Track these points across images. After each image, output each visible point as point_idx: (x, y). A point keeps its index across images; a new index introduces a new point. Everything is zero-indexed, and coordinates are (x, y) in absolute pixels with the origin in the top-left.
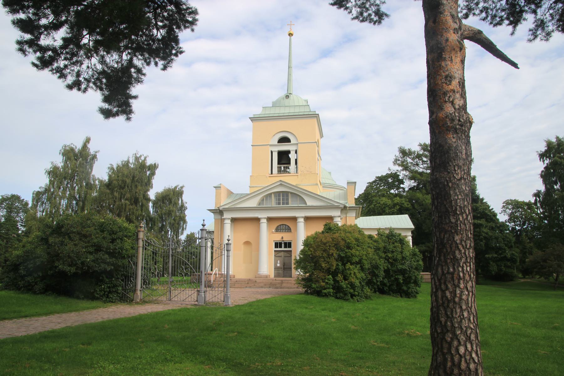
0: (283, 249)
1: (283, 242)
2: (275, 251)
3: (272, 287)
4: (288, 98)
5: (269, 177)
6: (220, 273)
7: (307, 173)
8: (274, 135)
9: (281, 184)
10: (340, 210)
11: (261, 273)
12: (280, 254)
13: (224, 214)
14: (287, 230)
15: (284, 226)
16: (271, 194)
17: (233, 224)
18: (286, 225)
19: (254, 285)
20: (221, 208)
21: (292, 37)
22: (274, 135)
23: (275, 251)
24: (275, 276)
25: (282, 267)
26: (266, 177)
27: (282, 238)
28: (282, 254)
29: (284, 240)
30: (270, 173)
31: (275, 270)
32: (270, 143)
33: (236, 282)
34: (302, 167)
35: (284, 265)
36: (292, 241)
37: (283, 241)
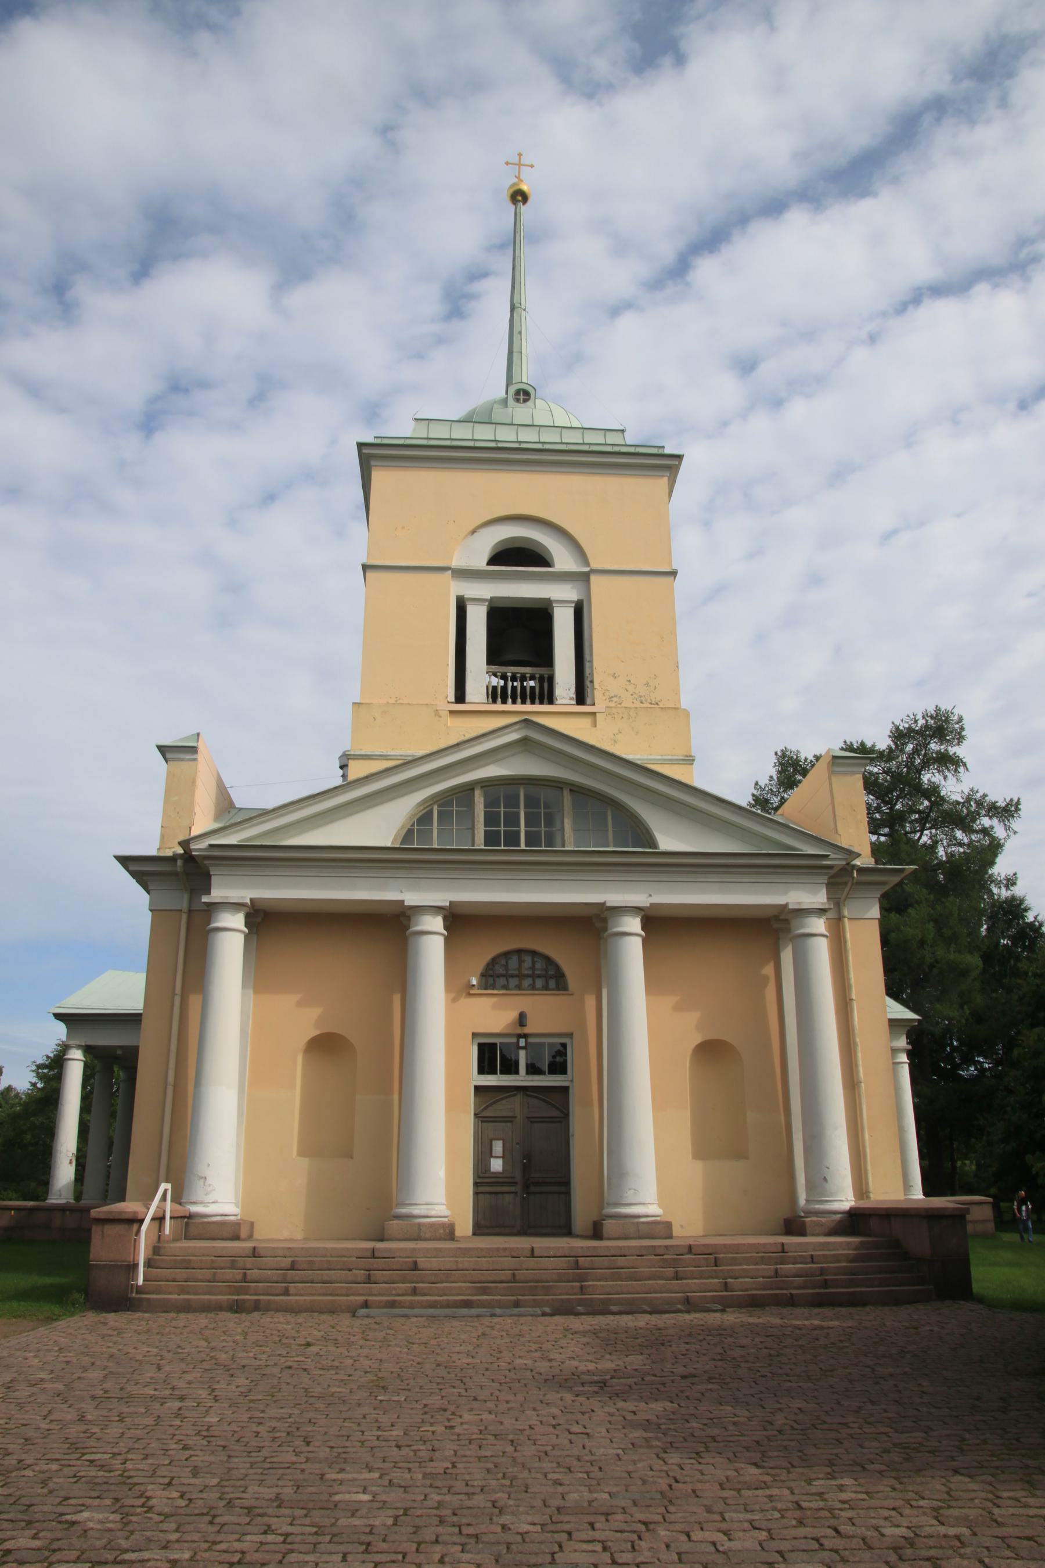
0: (522, 1079)
1: (522, 1043)
2: (478, 1089)
3: (536, 1304)
4: (525, 401)
5: (451, 712)
6: (180, 1210)
7: (638, 704)
8: (474, 532)
9: (525, 741)
10: (824, 880)
11: (416, 1211)
12: (503, 1108)
13: (214, 880)
14: (527, 982)
15: (528, 961)
16: (468, 789)
17: (255, 937)
18: (534, 953)
19: (414, 1292)
20: (198, 847)
21: (523, 208)
22: (474, 532)
23: (478, 1089)
24: (479, 1229)
25: (518, 1175)
26: (437, 713)
27: (522, 1020)
28: (515, 1106)
29: (527, 1030)
30: (452, 698)
31: (476, 1194)
32: (455, 563)
33: (292, 1268)
34: (614, 676)
35: (526, 1168)
36: (570, 1035)
37: (525, 1036)
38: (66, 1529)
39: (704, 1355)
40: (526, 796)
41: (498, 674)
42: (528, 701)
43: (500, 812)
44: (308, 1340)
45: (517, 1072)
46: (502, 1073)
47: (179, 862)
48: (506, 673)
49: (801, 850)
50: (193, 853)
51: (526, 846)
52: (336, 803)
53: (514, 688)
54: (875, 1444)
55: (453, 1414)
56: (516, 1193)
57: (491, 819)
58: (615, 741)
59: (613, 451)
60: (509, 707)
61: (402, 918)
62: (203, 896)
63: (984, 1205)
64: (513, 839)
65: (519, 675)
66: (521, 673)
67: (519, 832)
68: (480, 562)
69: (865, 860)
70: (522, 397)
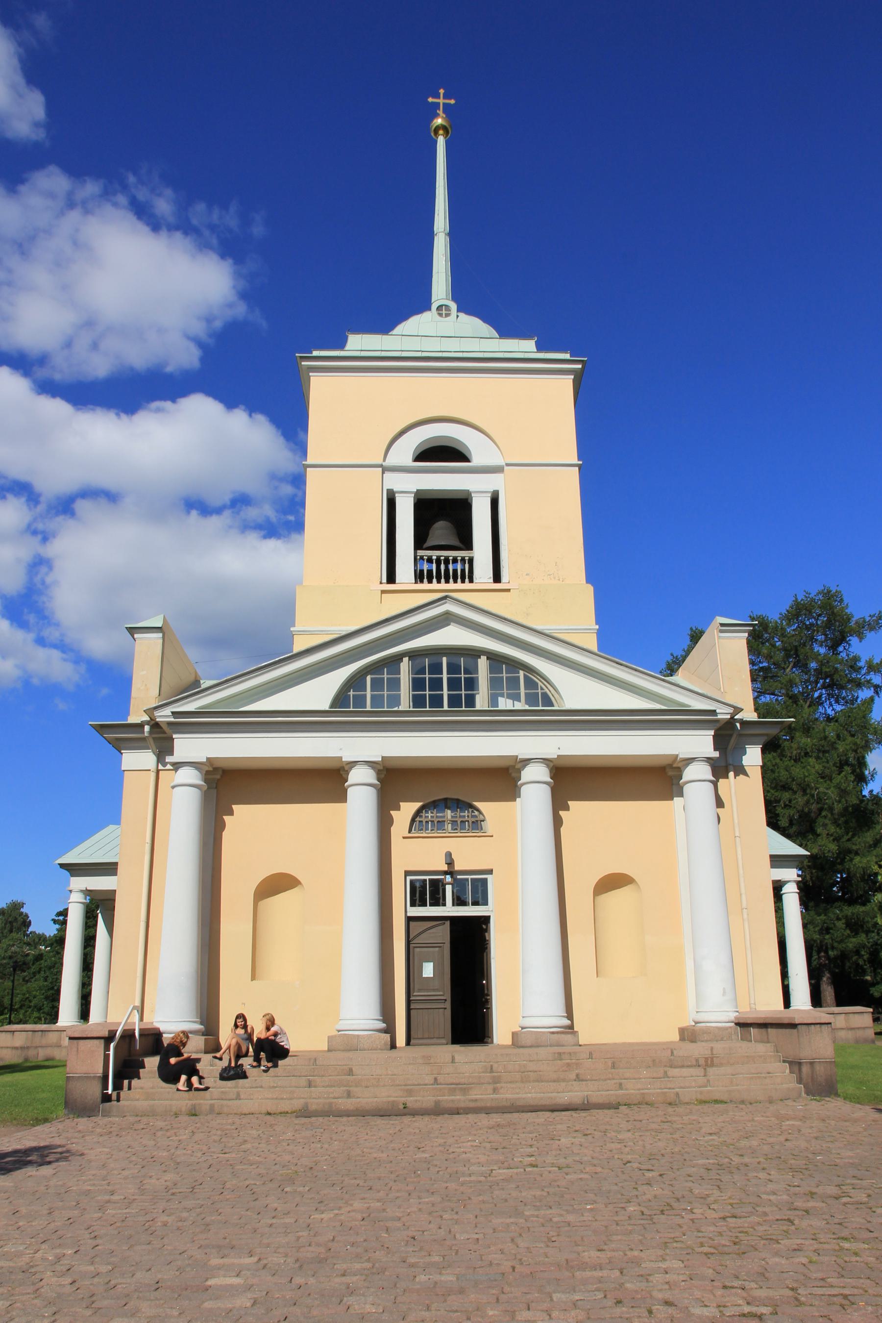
30: (384, 580)
38: (733, 1196)
39: (586, 1148)
40: (448, 664)
41: (425, 557)
42: (451, 580)
43: (384, 678)
44: (245, 1138)
45: (444, 905)
46: (431, 905)
47: (147, 728)
48: (432, 556)
49: (690, 706)
50: (157, 720)
51: (449, 706)
52: (614, 674)
53: (455, 571)
54: (712, 1228)
55: (346, 1203)
56: (445, 1008)
57: (417, 684)
58: (527, 614)
59: (545, 358)
60: (435, 585)
61: (341, 772)
62: (167, 757)
63: (865, 1014)
64: (437, 701)
65: (442, 558)
66: (445, 556)
67: (365, 696)
68: (407, 460)
69: (749, 714)
70: (444, 312)
